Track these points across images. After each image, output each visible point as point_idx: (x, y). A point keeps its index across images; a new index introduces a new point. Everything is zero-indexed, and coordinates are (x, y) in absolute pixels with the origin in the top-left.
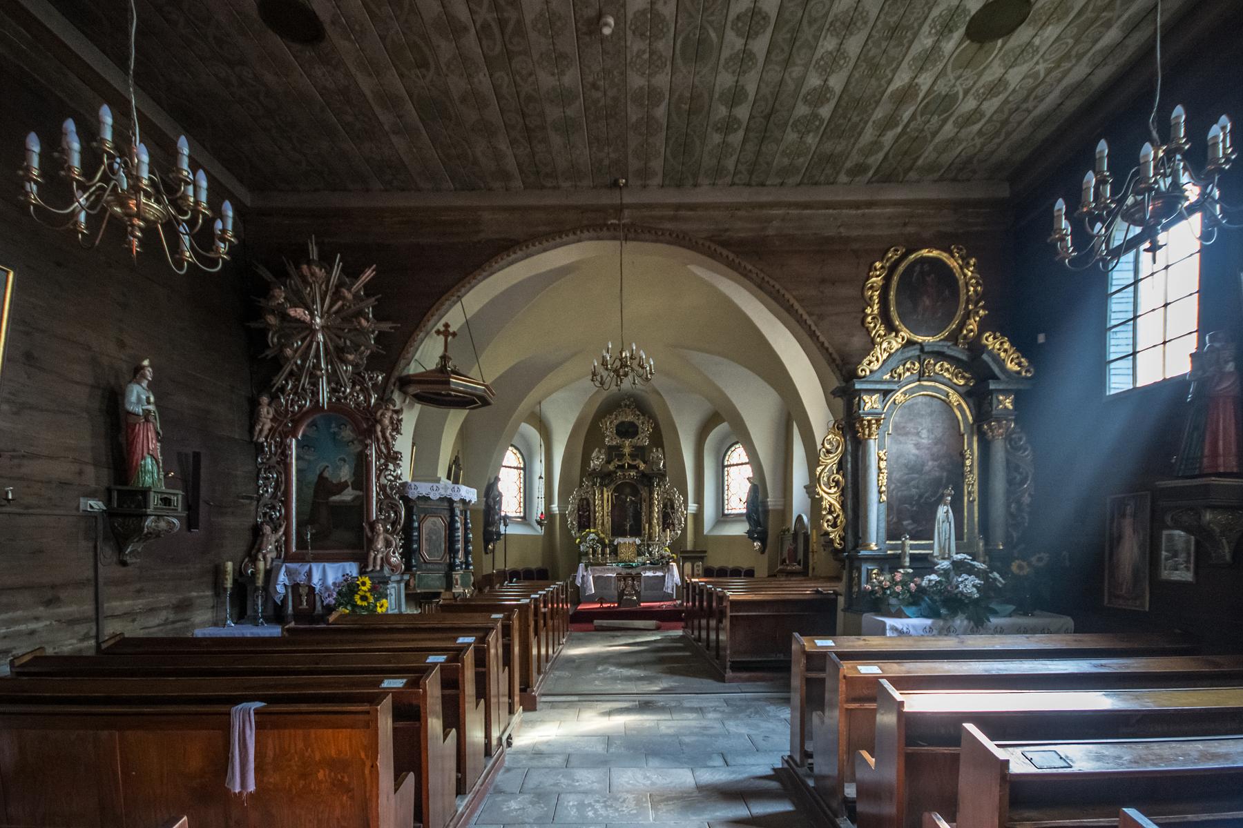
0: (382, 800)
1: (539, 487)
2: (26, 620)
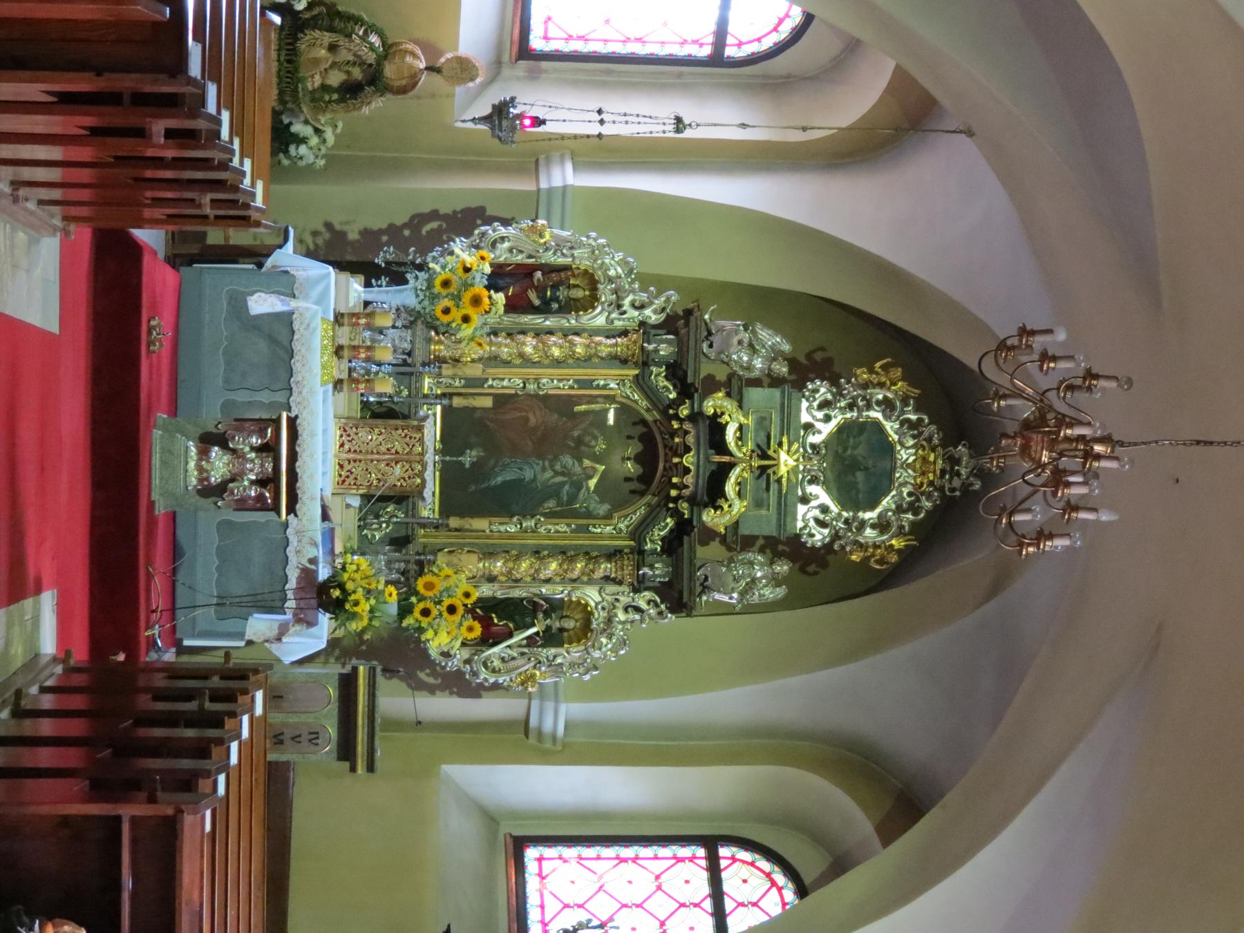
0: (162, 210)
1: (641, 115)
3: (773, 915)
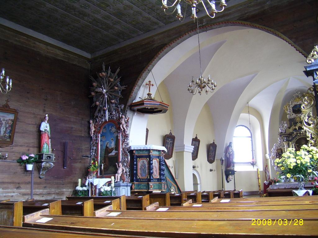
2: (11, 192)
3: (234, 138)
